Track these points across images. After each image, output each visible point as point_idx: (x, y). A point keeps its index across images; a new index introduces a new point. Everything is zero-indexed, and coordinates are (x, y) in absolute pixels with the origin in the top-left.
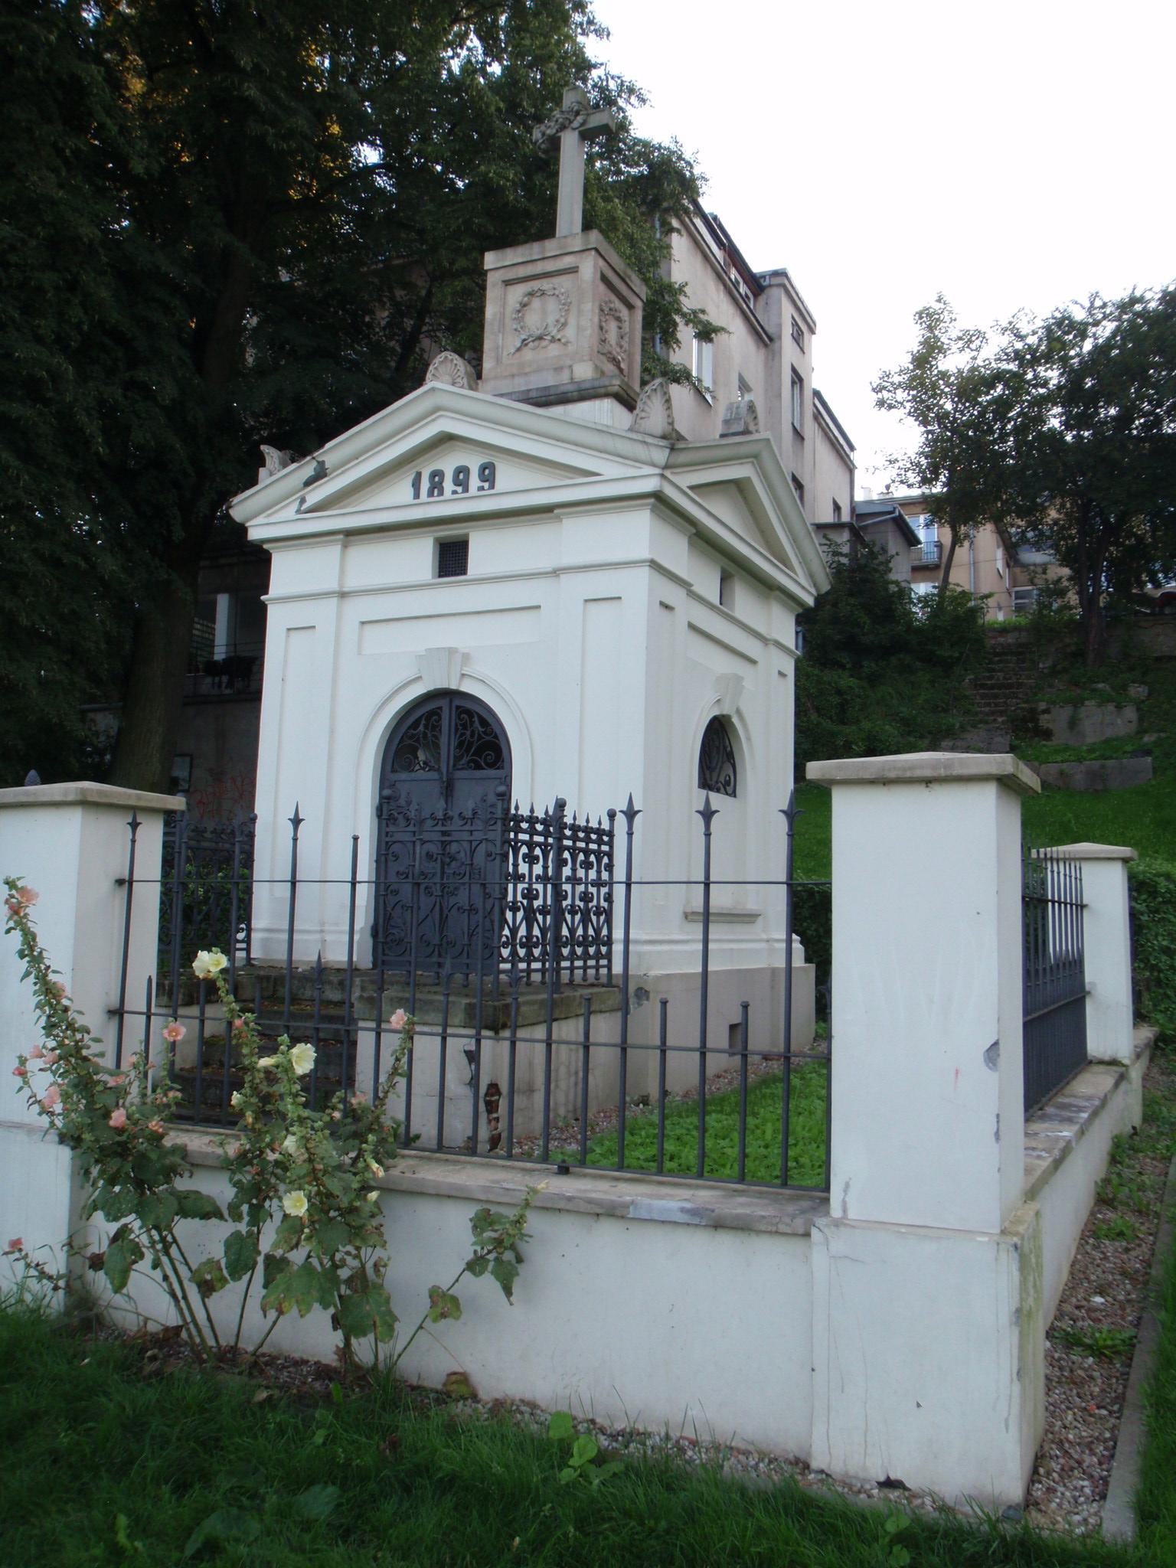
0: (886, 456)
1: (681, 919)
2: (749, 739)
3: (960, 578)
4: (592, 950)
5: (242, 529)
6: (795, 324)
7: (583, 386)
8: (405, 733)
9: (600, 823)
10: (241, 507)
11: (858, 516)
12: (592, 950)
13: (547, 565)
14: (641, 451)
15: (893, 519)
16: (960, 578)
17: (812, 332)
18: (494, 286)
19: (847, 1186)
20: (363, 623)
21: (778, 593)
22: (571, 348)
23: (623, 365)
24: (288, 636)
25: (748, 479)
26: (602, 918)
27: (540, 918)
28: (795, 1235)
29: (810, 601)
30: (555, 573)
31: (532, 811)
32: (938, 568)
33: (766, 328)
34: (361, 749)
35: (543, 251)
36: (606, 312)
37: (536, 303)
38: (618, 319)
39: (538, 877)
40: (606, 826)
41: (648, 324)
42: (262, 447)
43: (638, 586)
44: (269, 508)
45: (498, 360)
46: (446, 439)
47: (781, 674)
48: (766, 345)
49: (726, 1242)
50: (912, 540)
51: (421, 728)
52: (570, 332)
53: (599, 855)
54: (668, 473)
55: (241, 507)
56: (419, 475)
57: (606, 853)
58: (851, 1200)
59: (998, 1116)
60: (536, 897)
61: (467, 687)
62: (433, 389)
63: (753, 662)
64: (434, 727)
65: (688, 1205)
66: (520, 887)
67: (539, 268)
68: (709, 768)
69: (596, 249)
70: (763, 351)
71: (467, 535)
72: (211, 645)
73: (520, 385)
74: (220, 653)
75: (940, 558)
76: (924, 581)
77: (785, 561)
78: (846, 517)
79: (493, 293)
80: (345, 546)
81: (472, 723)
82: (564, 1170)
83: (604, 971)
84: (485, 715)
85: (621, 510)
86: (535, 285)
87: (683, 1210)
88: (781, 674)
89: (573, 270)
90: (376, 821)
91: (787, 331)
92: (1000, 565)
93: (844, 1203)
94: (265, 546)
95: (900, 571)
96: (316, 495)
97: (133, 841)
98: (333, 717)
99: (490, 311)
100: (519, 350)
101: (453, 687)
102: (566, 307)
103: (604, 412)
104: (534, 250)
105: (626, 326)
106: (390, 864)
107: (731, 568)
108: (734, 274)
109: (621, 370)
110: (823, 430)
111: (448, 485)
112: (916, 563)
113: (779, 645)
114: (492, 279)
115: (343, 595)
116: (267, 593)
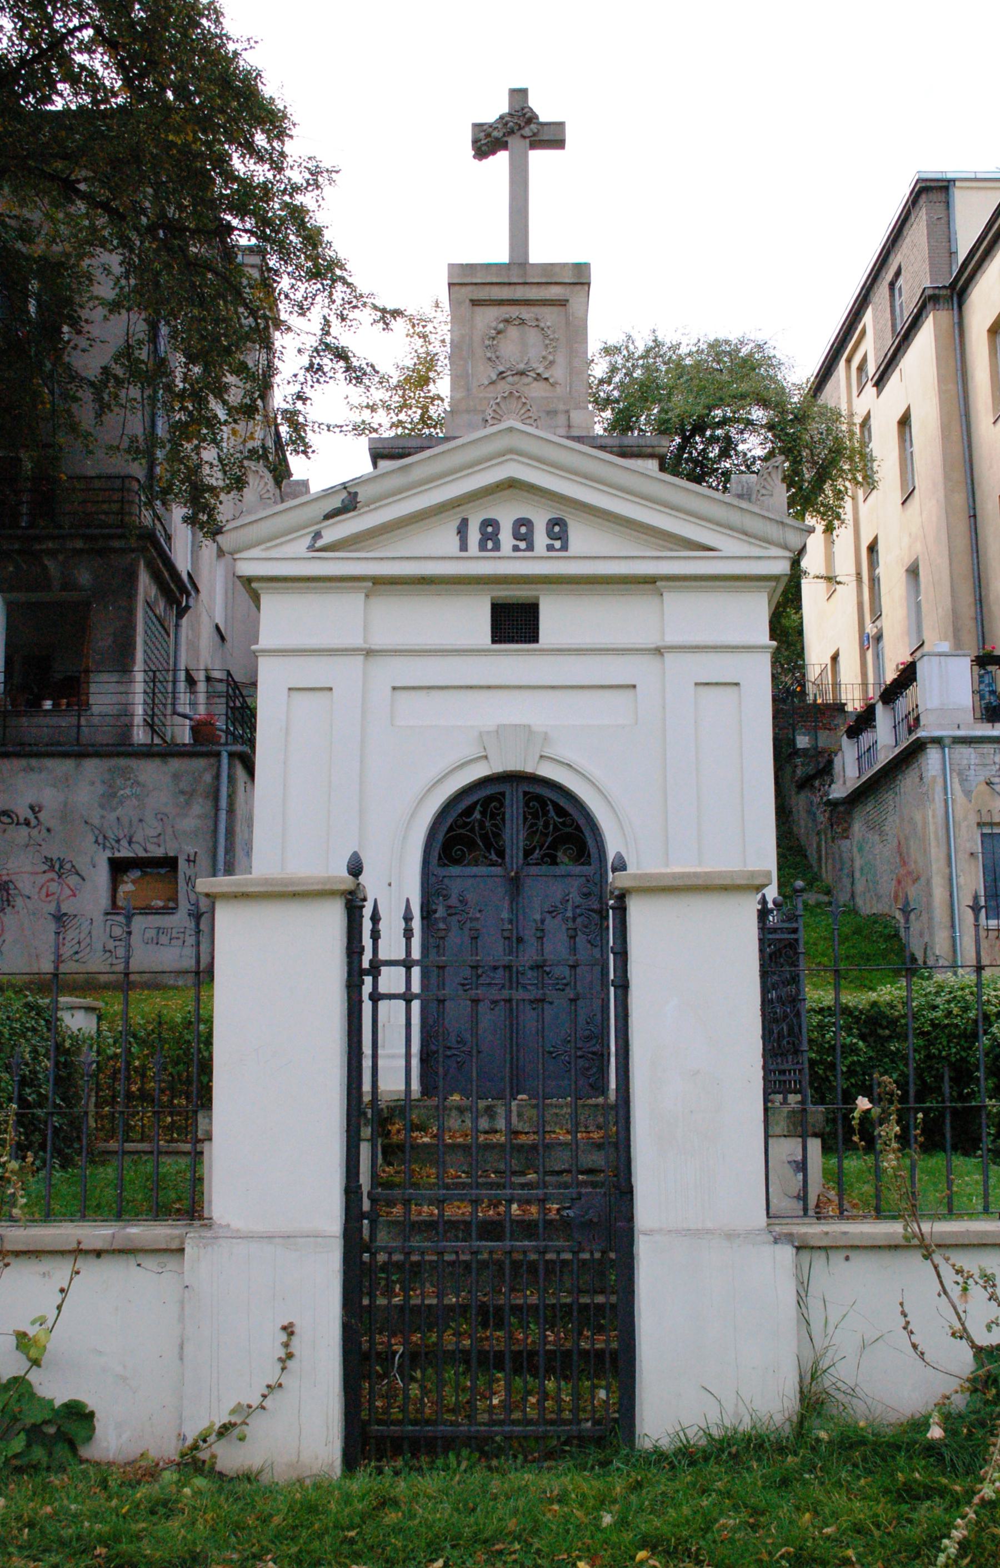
8: (455, 821)
13: (652, 640)
20: (394, 688)
22: (558, 389)
30: (658, 651)
44: (270, 540)
46: (512, 484)
51: (477, 815)
56: (465, 522)
62: (511, 429)
64: (493, 816)
71: (538, 598)
80: (367, 596)
81: (546, 813)
85: (737, 590)
86: (513, 311)
96: (333, 532)
100: (493, 383)
101: (529, 769)
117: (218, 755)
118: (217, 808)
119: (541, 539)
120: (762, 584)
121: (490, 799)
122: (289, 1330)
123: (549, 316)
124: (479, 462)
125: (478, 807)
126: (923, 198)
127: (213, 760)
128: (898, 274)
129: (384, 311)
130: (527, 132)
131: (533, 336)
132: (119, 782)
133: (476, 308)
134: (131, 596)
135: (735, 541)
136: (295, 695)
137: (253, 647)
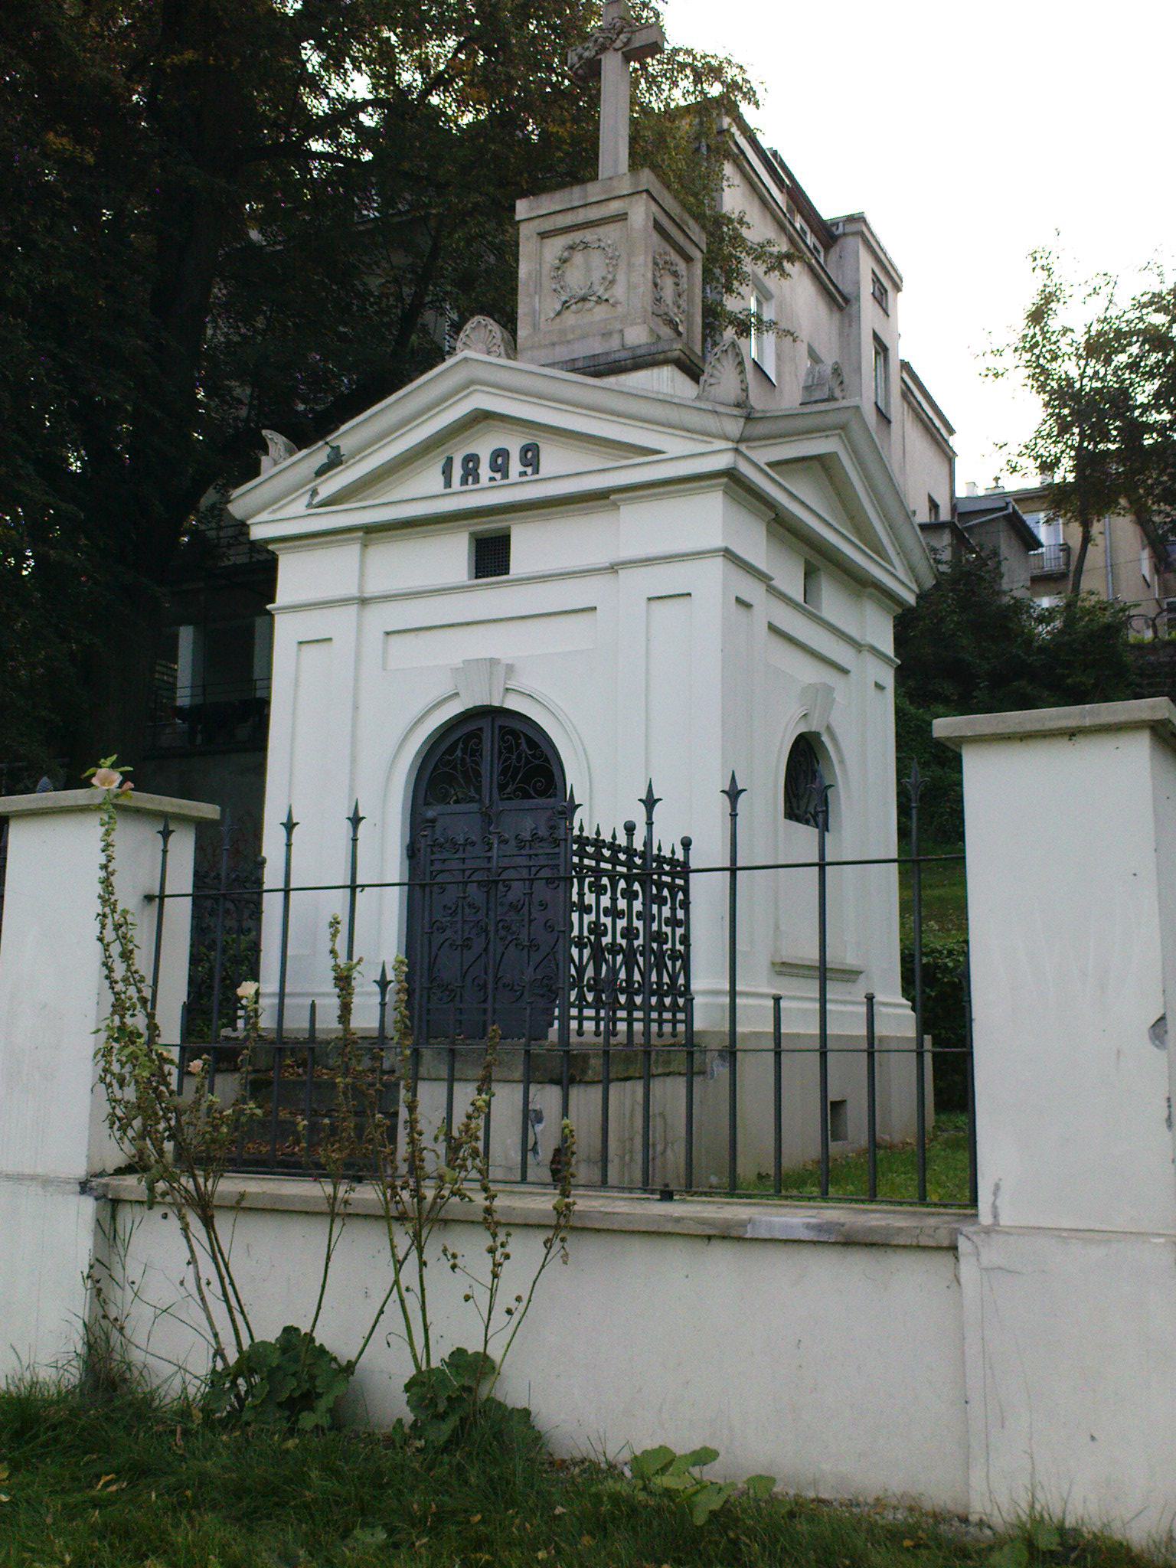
0: (998, 441)
1: (777, 948)
2: (842, 762)
3: (1094, 584)
4: (667, 1001)
5: (243, 527)
6: (876, 280)
7: (639, 352)
8: (440, 759)
9: (673, 852)
10: (242, 502)
11: (960, 514)
12: (667, 1001)
13: (604, 559)
14: (710, 423)
15: (1006, 516)
16: (1094, 584)
17: (898, 288)
18: (528, 239)
19: (997, 1188)
20: (388, 633)
21: (872, 590)
22: (620, 309)
23: (680, 328)
24: (299, 650)
25: (833, 456)
26: (679, 963)
27: (610, 957)
28: (939, 1248)
29: (911, 599)
30: (613, 568)
31: (598, 833)
32: (1064, 576)
33: (841, 287)
34: (388, 779)
35: (586, 197)
36: (660, 266)
37: (578, 258)
38: (675, 274)
39: (606, 909)
40: (680, 855)
41: (708, 276)
42: (264, 432)
43: (710, 581)
45: (535, 326)
46: (481, 418)
47: (879, 687)
48: (841, 309)
49: (858, 1262)
50: (1031, 542)
51: (459, 753)
52: (619, 292)
53: (672, 888)
54: (743, 447)
55: (242, 502)
56: (450, 460)
57: (680, 888)
58: (1003, 1202)
59: (1169, 1099)
60: (605, 934)
61: (513, 703)
62: (466, 360)
63: (844, 671)
65: (813, 1221)
66: (587, 918)
67: (581, 216)
68: (796, 796)
69: (647, 191)
70: (837, 315)
71: (509, 528)
72: (172, 688)
73: (562, 353)
74: (184, 698)
75: (1068, 564)
76: (1047, 594)
77: (880, 551)
78: (945, 515)
79: (527, 248)
80: (365, 546)
81: (518, 745)
82: (667, 1196)
83: (681, 1027)
84: (530, 733)
87: (808, 1226)
88: (879, 687)
89: (622, 217)
90: (407, 863)
91: (867, 288)
92: (1146, 568)
93: (994, 1207)
94: (270, 547)
95: (1014, 580)
96: (329, 487)
97: (165, 852)
98: (354, 741)
99: (524, 270)
100: (559, 314)
102: (613, 261)
103: (665, 380)
104: (574, 195)
105: (684, 282)
106: (434, 896)
107: (817, 560)
108: (799, 222)
109: (679, 334)
110: (914, 409)
111: (485, 471)
112: (1037, 572)
113: (874, 651)
114: (525, 231)
115: (363, 601)
116: (272, 600)
120: (713, 482)
121: (469, 736)
124: (444, 399)
125: (461, 745)
133: (546, 241)
135: (678, 440)
136: (304, 647)
137: (269, 607)
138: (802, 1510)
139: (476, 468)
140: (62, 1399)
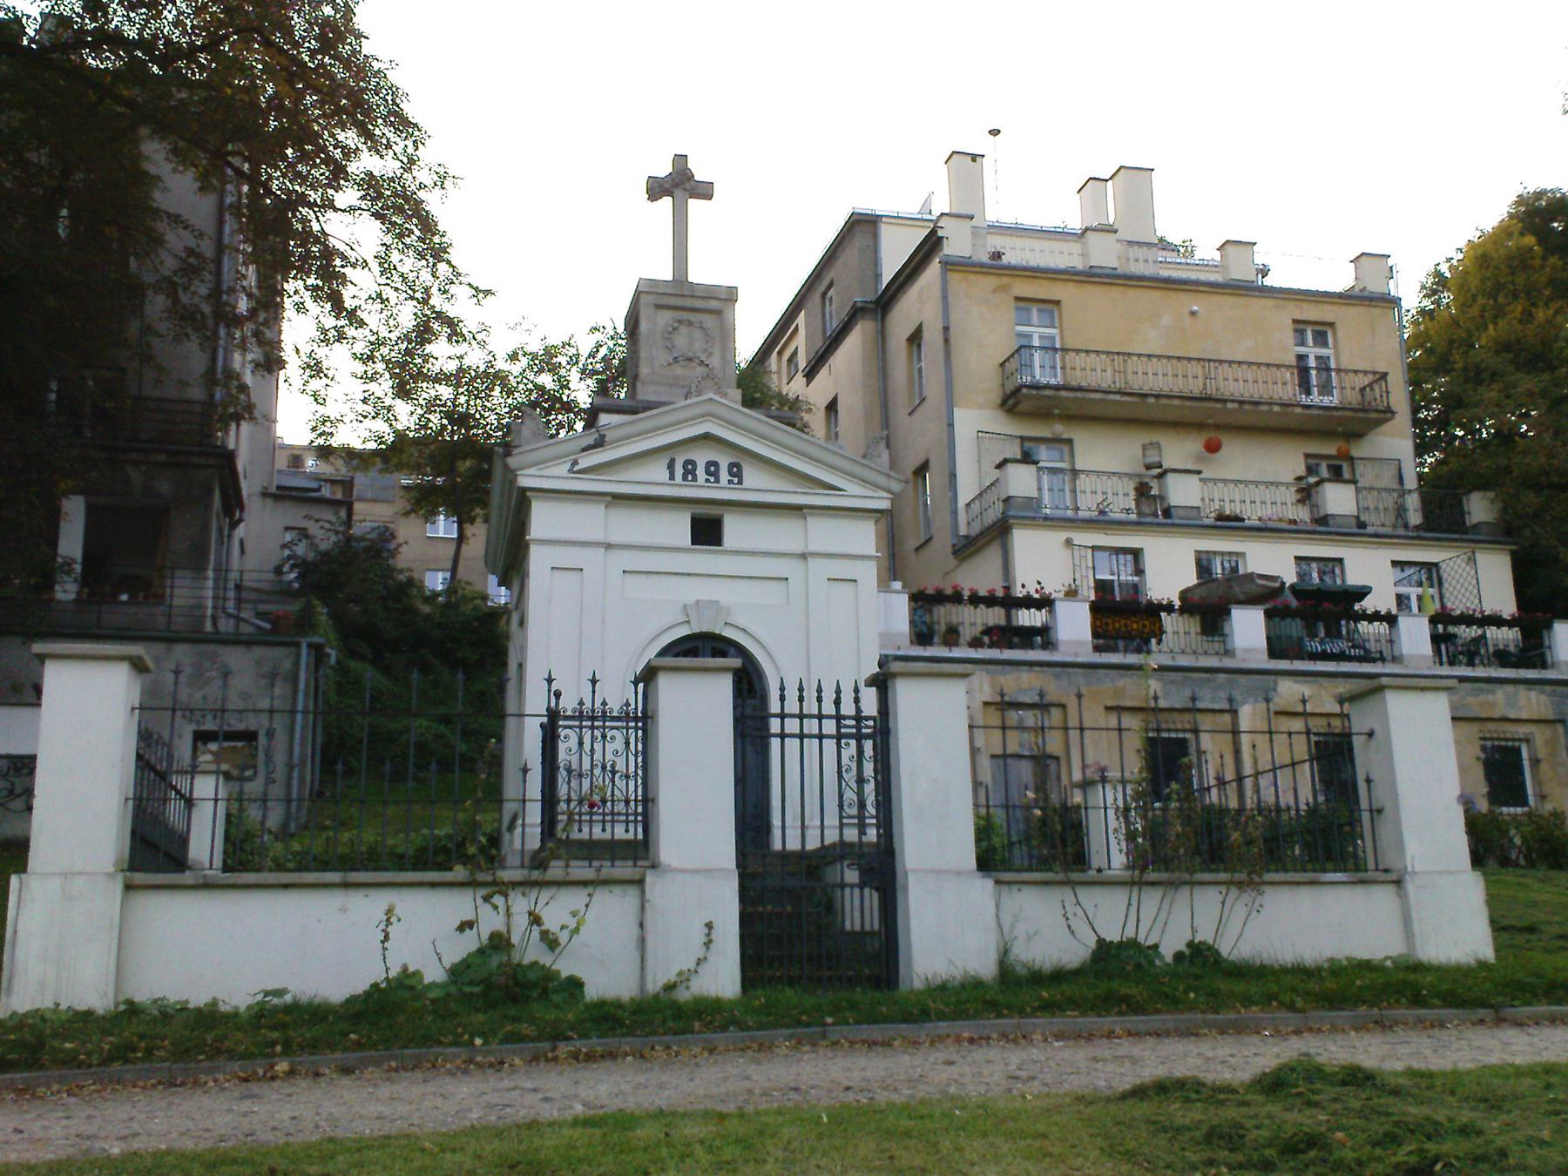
30: (804, 556)
46: (707, 437)
85: (855, 518)
86: (685, 315)
117: (298, 645)
118: (295, 692)
119: (724, 476)
122: (709, 926)
123: (709, 321)
126: (857, 229)
127: (293, 649)
128: (830, 285)
129: (476, 289)
130: (687, 186)
131: (697, 334)
132: (207, 665)
134: (208, 507)
138: (943, 987)
139: (695, 469)
140: (730, 1001)
